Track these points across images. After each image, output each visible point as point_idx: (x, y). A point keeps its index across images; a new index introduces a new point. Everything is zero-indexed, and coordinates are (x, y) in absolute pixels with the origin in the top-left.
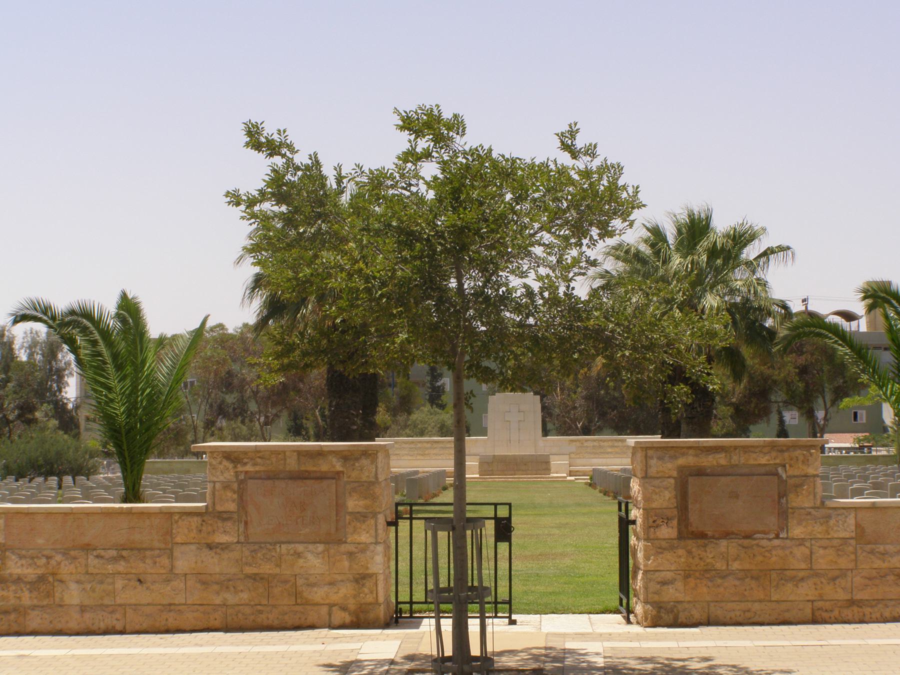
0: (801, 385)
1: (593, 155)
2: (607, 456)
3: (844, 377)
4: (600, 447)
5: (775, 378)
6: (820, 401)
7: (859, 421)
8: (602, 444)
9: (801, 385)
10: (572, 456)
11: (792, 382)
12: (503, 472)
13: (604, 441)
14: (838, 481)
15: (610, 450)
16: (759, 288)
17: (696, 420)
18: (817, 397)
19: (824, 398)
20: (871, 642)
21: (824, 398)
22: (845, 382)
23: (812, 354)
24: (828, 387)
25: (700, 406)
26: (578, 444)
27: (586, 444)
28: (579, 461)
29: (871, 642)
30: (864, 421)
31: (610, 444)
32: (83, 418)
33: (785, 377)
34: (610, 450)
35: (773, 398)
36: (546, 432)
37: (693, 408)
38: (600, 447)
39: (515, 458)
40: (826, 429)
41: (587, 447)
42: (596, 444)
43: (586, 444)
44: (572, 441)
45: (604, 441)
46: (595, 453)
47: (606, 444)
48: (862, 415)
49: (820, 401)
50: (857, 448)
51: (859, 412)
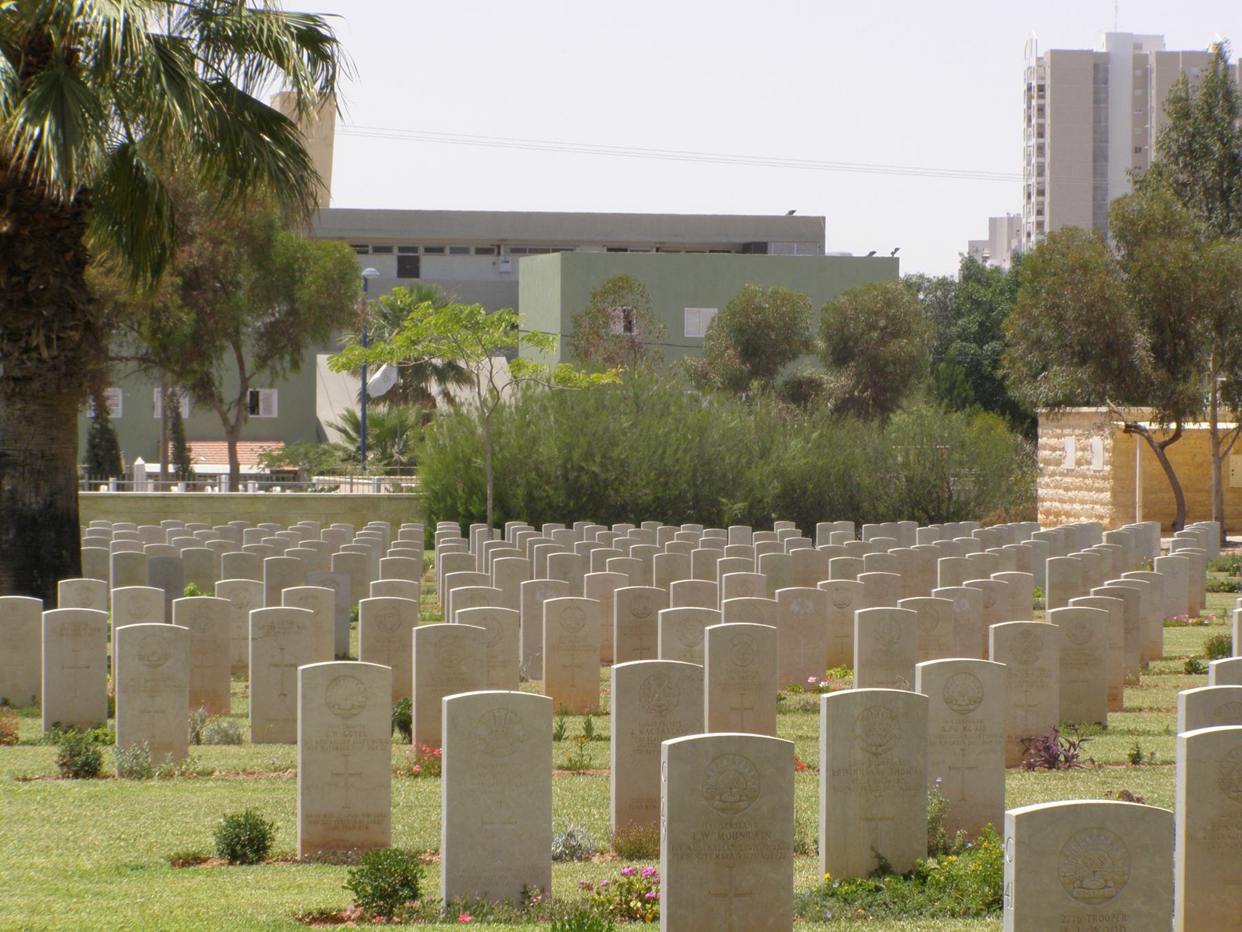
0: (187, 317)
3: (291, 300)
6: (229, 356)
7: (262, 414)
9: (188, 317)
11: (166, 307)
14: (472, 598)
16: (18, 86)
17: (35, 386)
18: (222, 348)
19: (237, 348)
21: (237, 348)
22: (292, 312)
23: (216, 242)
24: (254, 324)
25: (49, 343)
30: (275, 414)
35: (113, 349)
37: (27, 350)
40: (244, 429)
48: (268, 398)
49: (229, 356)
50: (267, 478)
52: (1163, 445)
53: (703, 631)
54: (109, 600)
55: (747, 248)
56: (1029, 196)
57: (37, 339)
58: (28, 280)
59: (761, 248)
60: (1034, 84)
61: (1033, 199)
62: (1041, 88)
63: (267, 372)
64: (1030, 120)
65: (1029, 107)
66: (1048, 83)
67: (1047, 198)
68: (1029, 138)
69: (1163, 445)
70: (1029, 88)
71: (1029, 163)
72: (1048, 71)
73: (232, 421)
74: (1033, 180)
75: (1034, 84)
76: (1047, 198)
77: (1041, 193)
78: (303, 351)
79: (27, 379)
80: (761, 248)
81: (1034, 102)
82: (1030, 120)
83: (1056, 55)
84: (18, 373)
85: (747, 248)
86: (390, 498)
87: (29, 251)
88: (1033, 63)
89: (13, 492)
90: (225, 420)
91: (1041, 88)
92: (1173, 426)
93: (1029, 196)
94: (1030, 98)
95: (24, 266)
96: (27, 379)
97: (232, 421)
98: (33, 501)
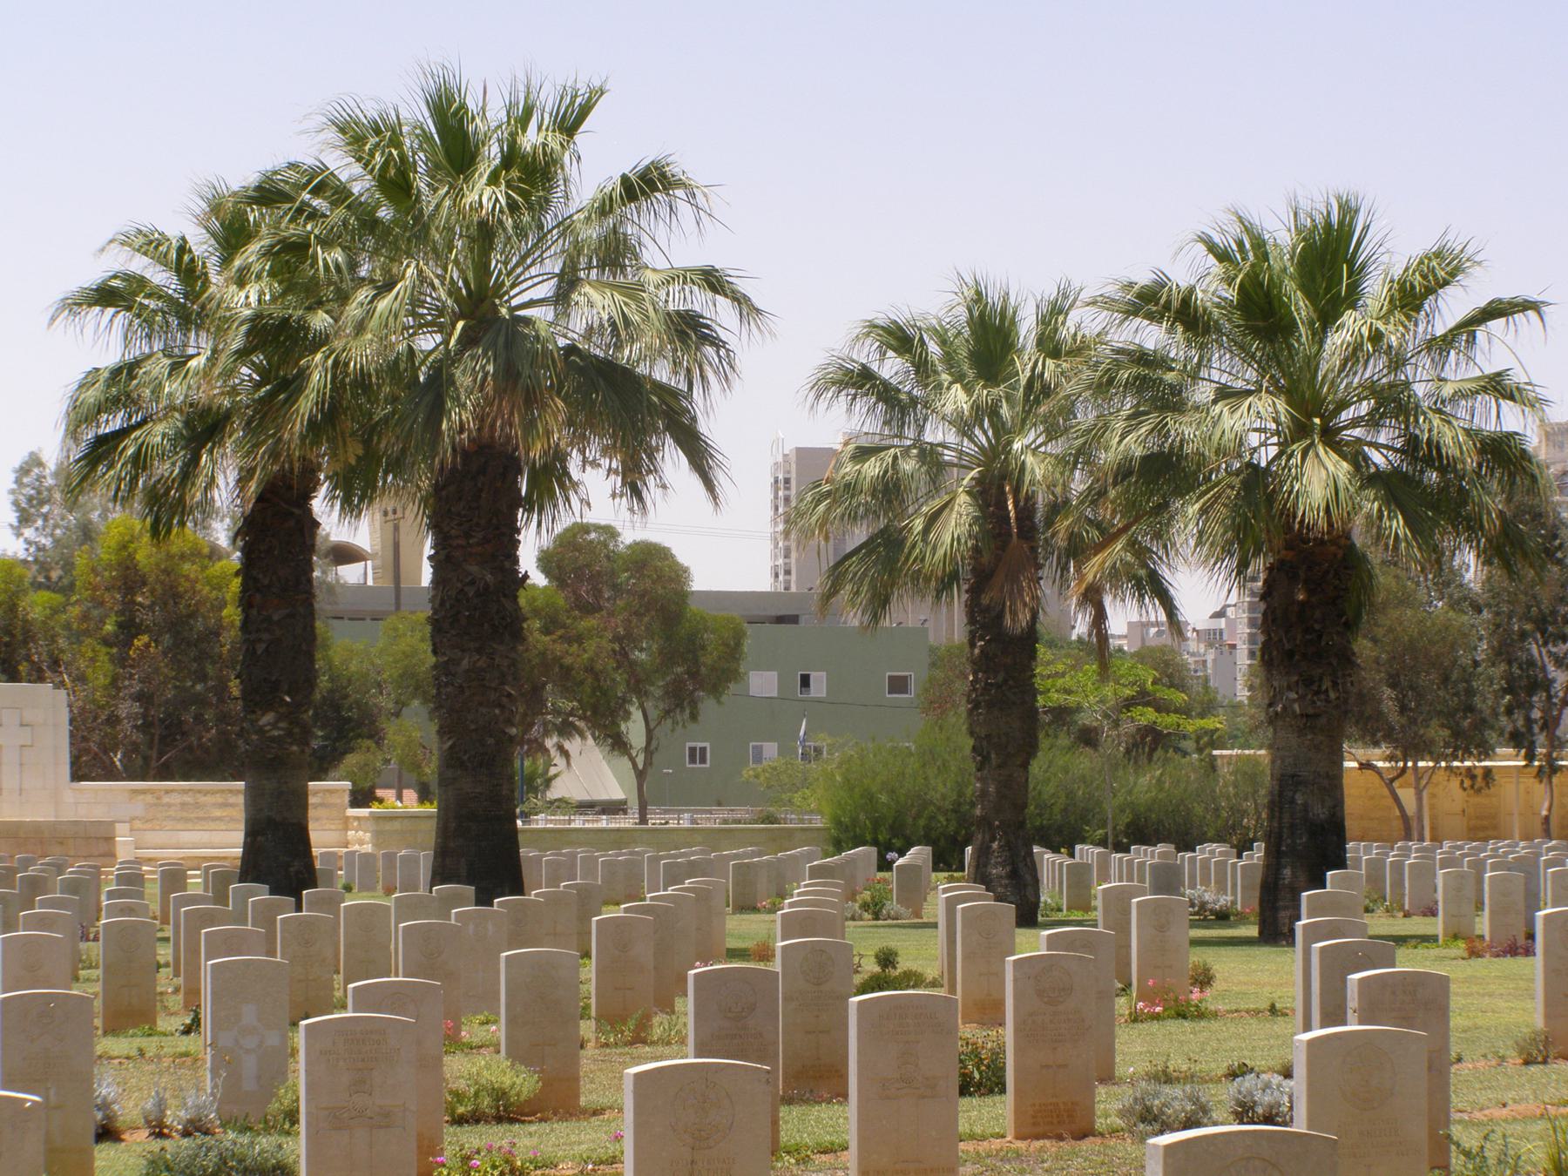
1: (40, 464)
2: (212, 825)
4: (197, 805)
5: (568, 660)
6: (637, 715)
8: (202, 799)
10: (138, 824)
12: (745, 950)
13: (206, 793)
15: (218, 813)
17: (1323, 720)
20: (1012, 514)
26: (149, 798)
27: (166, 799)
28: (151, 837)
29: (1012, 514)
31: (219, 799)
32: (892, 944)
33: (591, 660)
34: (218, 813)
36: (78, 775)
37: (1317, 693)
38: (197, 805)
39: (36, 827)
41: (169, 805)
42: (188, 799)
43: (166, 799)
44: (135, 792)
45: (206, 793)
46: (187, 820)
47: (209, 799)
51: (814, 676)
52: (1392, 780)
53: (498, 958)
54: (1480, 891)
55: (780, 620)
56: (777, 576)
57: (1327, 684)
58: (1320, 637)
59: (793, 619)
60: (781, 477)
61: (781, 578)
62: (787, 481)
63: (669, 721)
64: (777, 509)
65: (776, 497)
66: (793, 476)
67: (793, 577)
68: (776, 524)
69: (1392, 780)
70: (776, 481)
71: (776, 546)
72: (794, 466)
73: (640, 766)
74: (780, 561)
75: (781, 477)
76: (793, 577)
77: (788, 572)
78: (700, 705)
79: (1317, 716)
80: (793, 619)
81: (781, 493)
82: (777, 509)
83: (801, 452)
84: (1310, 711)
85: (780, 620)
86: (688, 830)
87: (1318, 614)
88: (780, 459)
89: (1305, 805)
90: (635, 765)
91: (787, 481)
92: (1401, 764)
93: (777, 576)
94: (776, 491)
95: (1317, 627)
96: (1317, 716)
97: (640, 766)
98: (1320, 812)
